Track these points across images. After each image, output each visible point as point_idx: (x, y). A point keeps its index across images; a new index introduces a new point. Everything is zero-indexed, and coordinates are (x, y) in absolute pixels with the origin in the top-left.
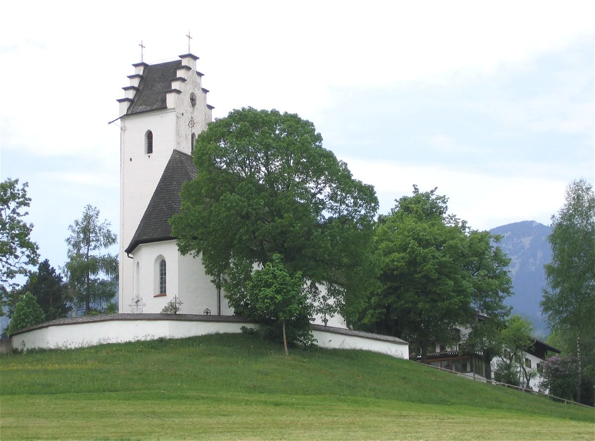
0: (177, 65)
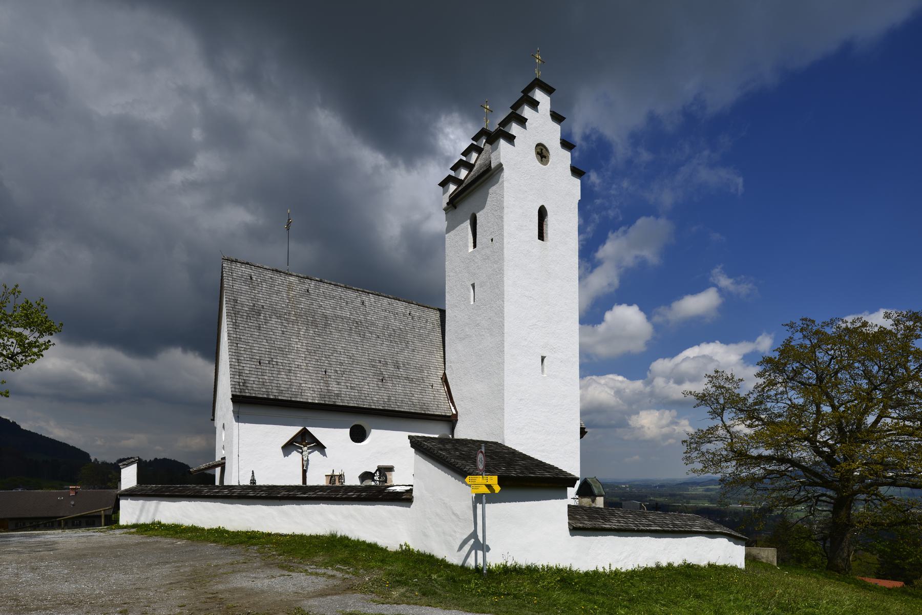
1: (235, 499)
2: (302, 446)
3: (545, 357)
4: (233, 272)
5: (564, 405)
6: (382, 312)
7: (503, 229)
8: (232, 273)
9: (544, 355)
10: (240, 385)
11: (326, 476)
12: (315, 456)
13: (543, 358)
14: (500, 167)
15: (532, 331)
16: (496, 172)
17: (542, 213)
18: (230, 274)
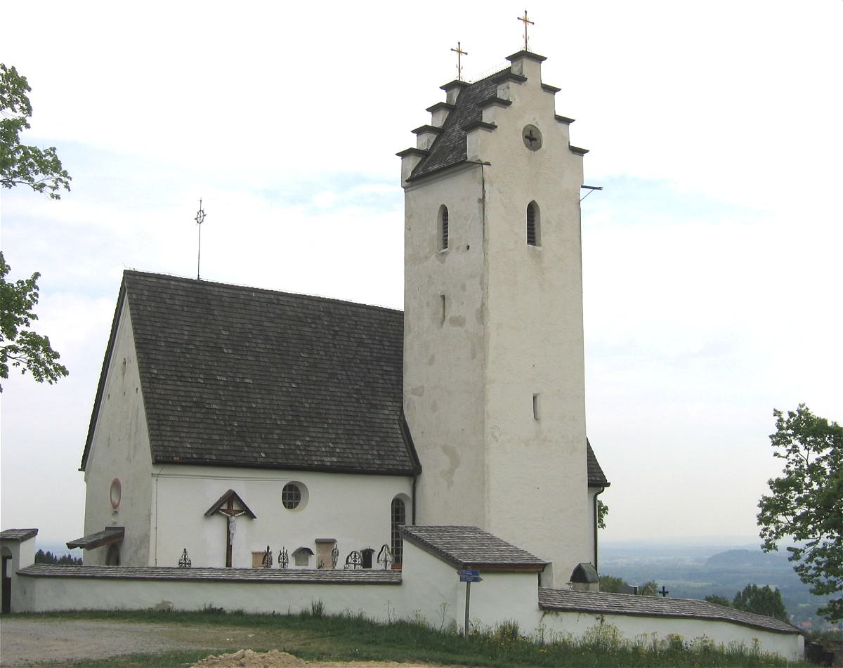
0: (503, 77)
3: (538, 394)
9: (535, 393)
12: (240, 524)
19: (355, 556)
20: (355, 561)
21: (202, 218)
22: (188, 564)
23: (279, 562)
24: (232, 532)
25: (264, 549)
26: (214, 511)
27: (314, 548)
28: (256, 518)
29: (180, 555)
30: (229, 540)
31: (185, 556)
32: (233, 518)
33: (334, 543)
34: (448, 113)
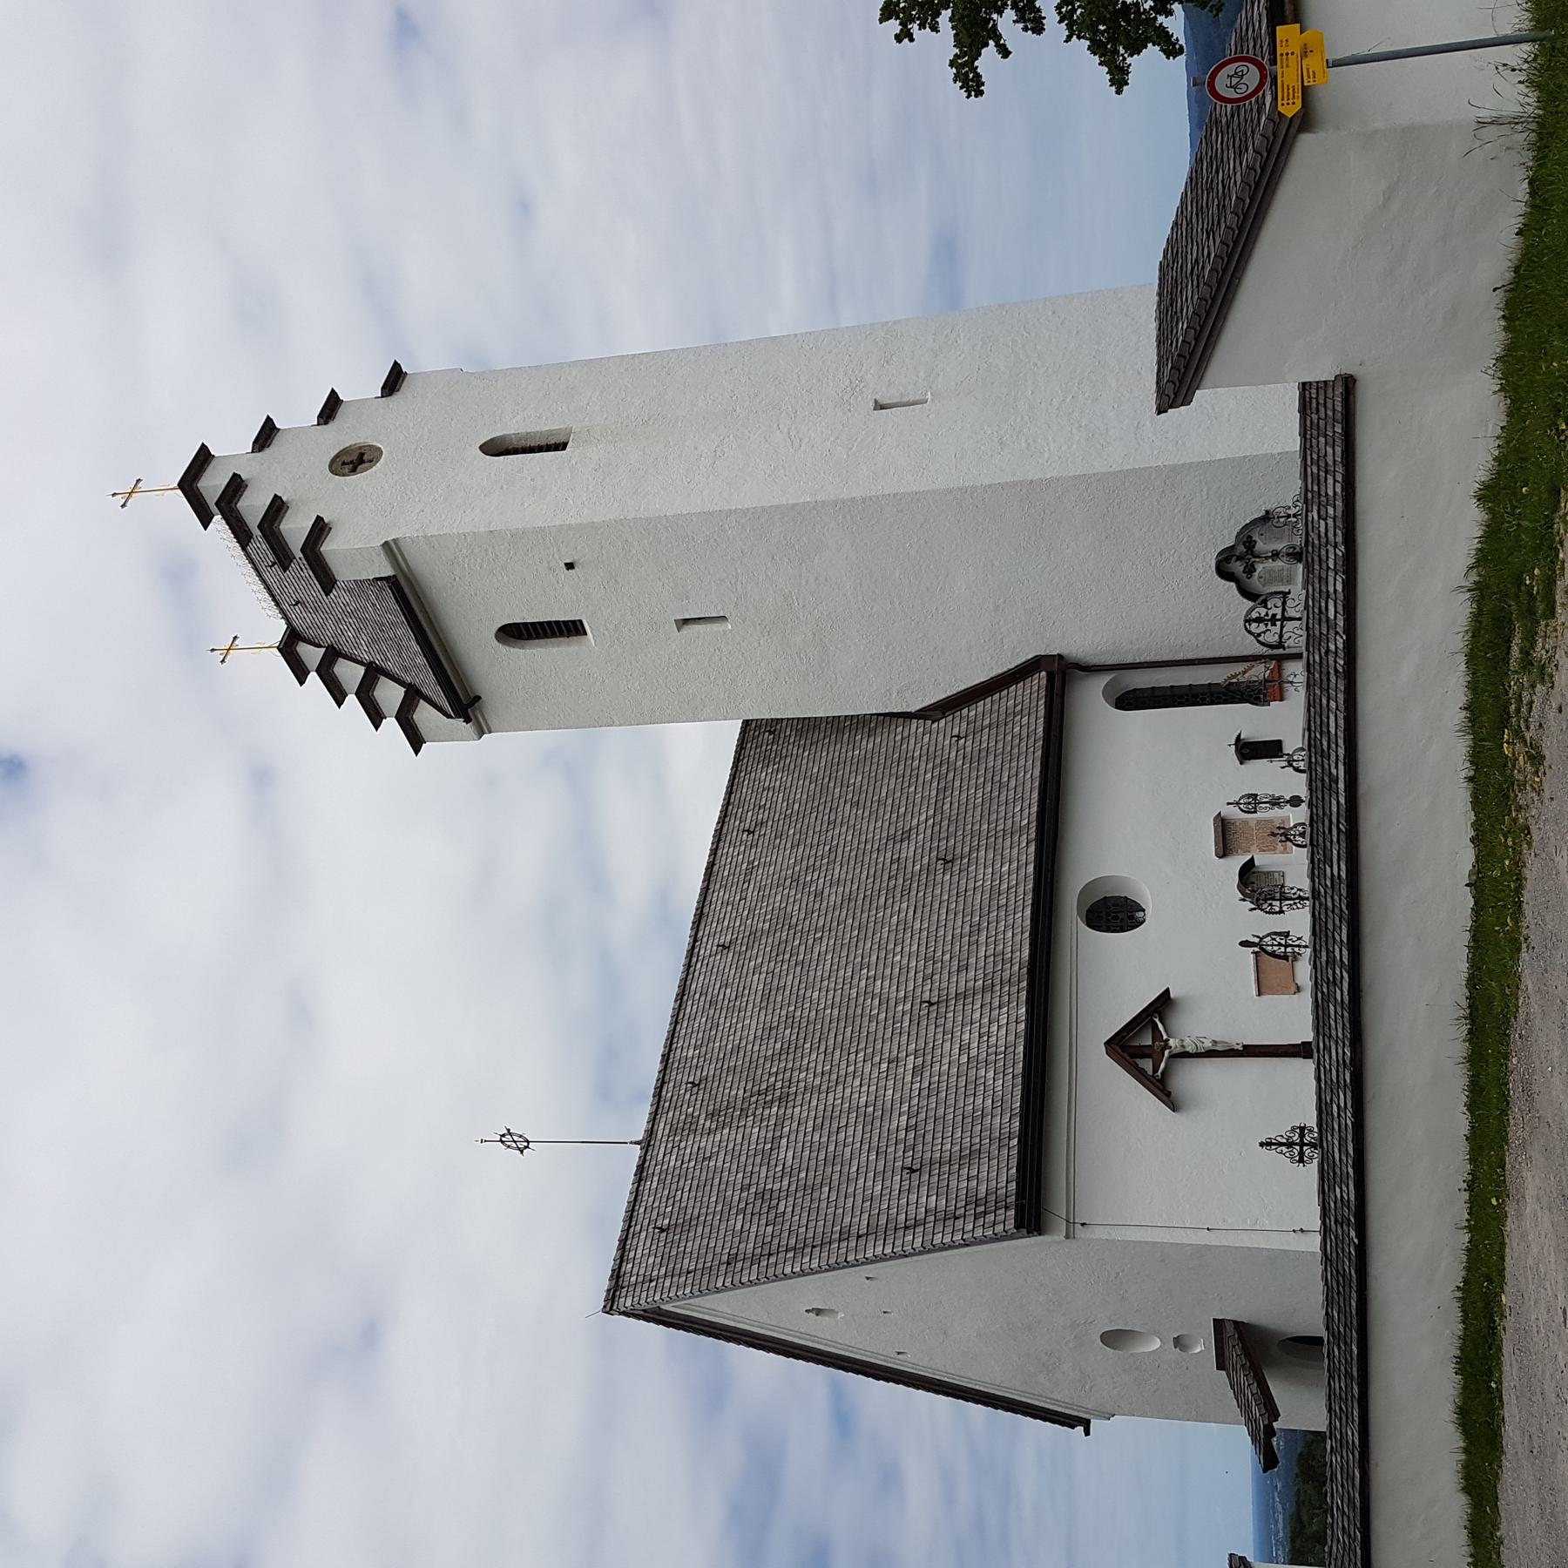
1: (1362, 1053)
2: (1167, 1052)
3: (876, 401)
4: (648, 1278)
5: (1014, 341)
6: (749, 899)
7: (542, 529)
8: (651, 1281)
9: (872, 404)
10: (985, 1213)
11: (1259, 994)
12: (1189, 1030)
13: (879, 406)
14: (390, 549)
15: (806, 440)
16: (404, 566)
17: (495, 448)
18: (653, 1284)
19: (1259, 620)
20: (1273, 620)
21: (516, 1138)
22: (1302, 1136)
23: (1281, 912)
24: (1208, 1044)
25: (1248, 954)
26: (1161, 1088)
27: (1238, 861)
28: (1167, 991)
29: (1279, 1161)
30: (1231, 1053)
31: (1281, 1144)
32: (1172, 1042)
33: (1223, 820)
34: (340, 659)
